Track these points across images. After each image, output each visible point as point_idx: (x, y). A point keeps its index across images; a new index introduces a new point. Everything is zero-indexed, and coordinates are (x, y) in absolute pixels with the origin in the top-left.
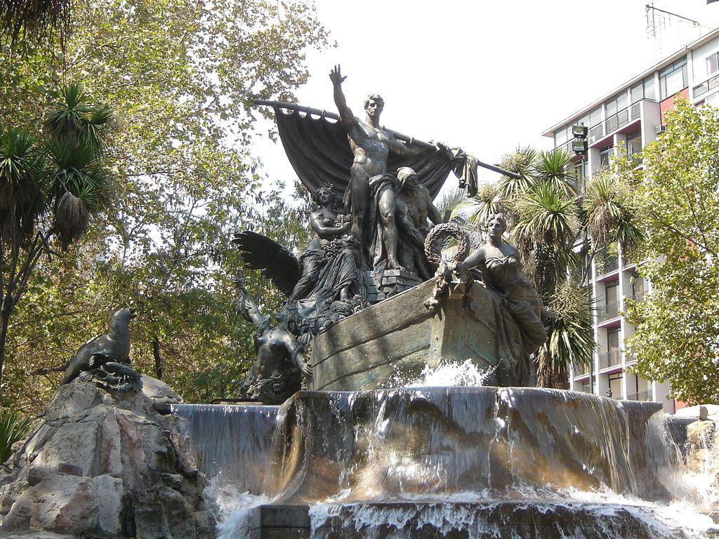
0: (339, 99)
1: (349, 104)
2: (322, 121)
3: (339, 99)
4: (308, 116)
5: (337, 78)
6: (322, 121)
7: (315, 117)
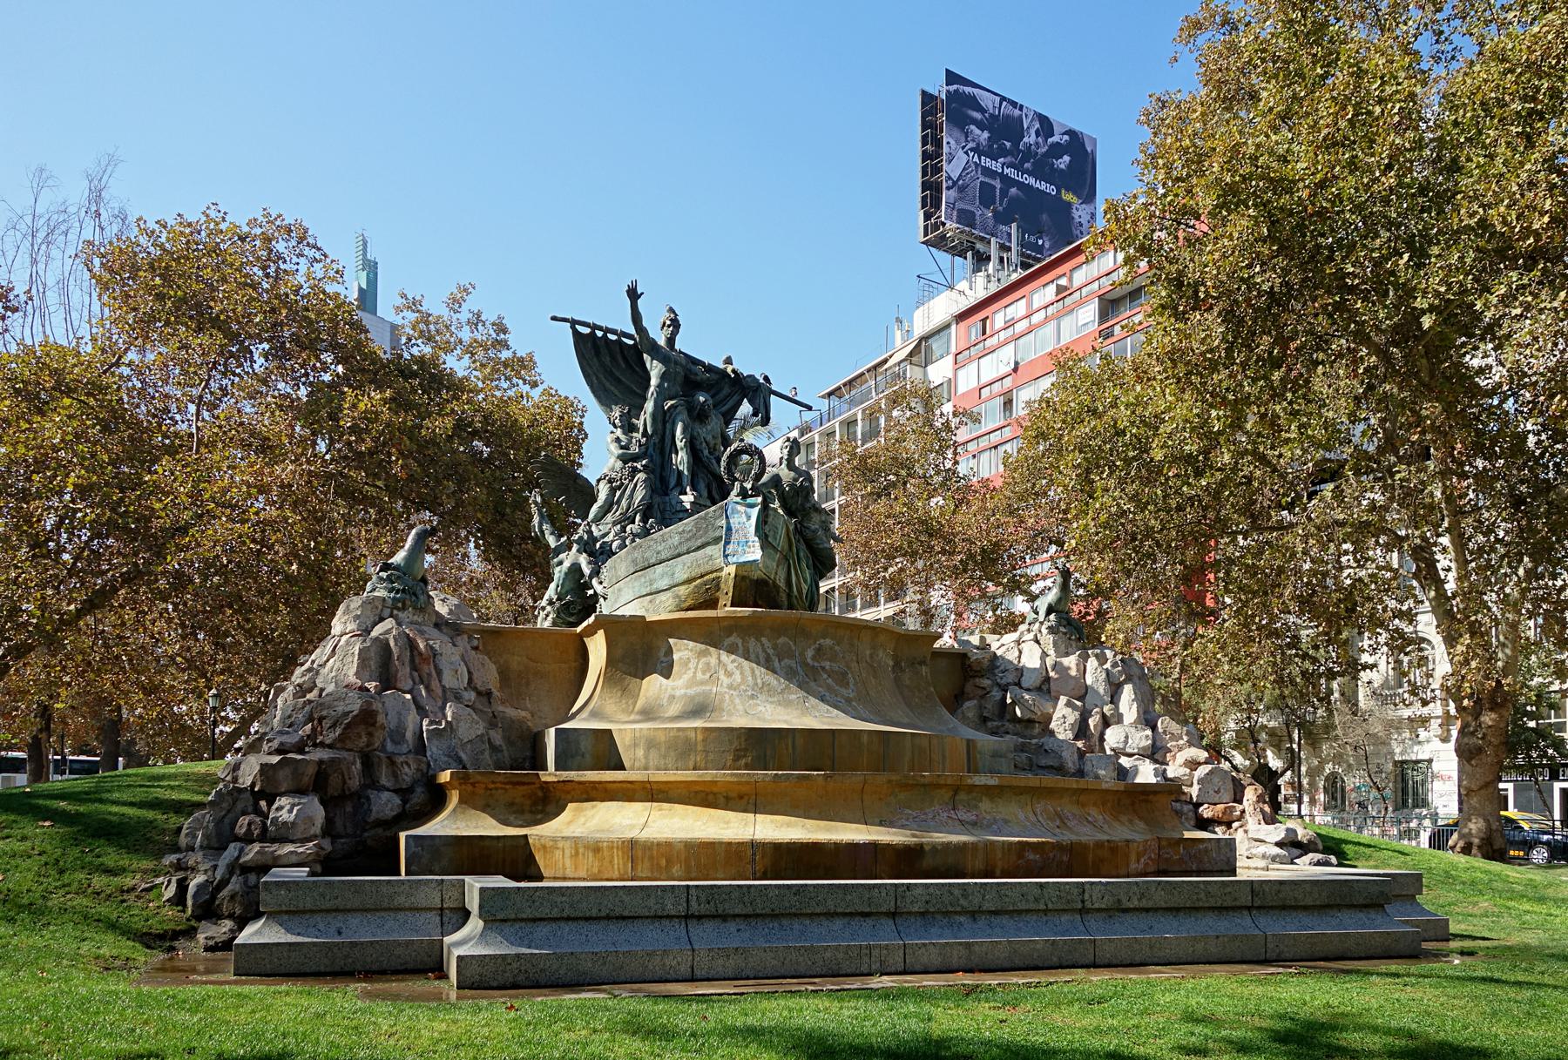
0: (636, 318)
1: (645, 324)
2: (619, 342)
3: (636, 318)
4: (605, 336)
5: (633, 294)
6: (619, 342)
7: (613, 337)
